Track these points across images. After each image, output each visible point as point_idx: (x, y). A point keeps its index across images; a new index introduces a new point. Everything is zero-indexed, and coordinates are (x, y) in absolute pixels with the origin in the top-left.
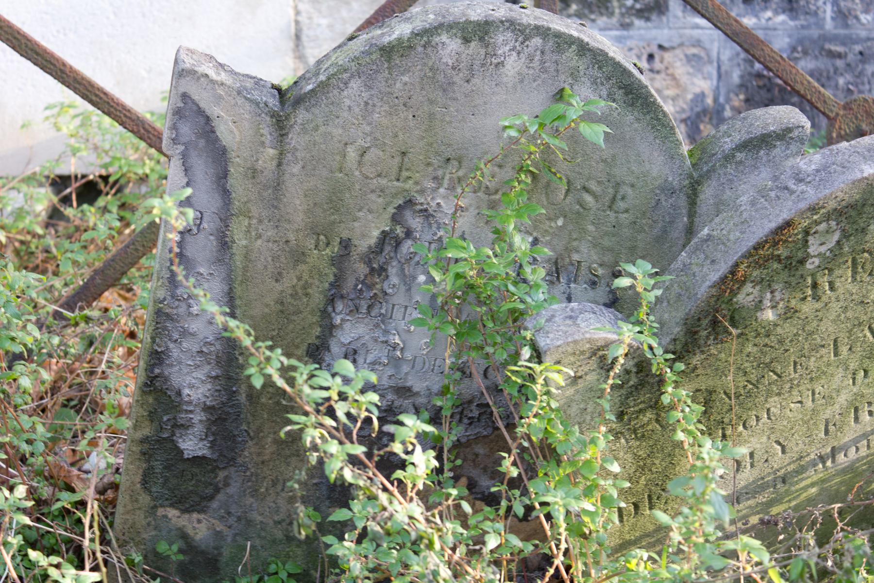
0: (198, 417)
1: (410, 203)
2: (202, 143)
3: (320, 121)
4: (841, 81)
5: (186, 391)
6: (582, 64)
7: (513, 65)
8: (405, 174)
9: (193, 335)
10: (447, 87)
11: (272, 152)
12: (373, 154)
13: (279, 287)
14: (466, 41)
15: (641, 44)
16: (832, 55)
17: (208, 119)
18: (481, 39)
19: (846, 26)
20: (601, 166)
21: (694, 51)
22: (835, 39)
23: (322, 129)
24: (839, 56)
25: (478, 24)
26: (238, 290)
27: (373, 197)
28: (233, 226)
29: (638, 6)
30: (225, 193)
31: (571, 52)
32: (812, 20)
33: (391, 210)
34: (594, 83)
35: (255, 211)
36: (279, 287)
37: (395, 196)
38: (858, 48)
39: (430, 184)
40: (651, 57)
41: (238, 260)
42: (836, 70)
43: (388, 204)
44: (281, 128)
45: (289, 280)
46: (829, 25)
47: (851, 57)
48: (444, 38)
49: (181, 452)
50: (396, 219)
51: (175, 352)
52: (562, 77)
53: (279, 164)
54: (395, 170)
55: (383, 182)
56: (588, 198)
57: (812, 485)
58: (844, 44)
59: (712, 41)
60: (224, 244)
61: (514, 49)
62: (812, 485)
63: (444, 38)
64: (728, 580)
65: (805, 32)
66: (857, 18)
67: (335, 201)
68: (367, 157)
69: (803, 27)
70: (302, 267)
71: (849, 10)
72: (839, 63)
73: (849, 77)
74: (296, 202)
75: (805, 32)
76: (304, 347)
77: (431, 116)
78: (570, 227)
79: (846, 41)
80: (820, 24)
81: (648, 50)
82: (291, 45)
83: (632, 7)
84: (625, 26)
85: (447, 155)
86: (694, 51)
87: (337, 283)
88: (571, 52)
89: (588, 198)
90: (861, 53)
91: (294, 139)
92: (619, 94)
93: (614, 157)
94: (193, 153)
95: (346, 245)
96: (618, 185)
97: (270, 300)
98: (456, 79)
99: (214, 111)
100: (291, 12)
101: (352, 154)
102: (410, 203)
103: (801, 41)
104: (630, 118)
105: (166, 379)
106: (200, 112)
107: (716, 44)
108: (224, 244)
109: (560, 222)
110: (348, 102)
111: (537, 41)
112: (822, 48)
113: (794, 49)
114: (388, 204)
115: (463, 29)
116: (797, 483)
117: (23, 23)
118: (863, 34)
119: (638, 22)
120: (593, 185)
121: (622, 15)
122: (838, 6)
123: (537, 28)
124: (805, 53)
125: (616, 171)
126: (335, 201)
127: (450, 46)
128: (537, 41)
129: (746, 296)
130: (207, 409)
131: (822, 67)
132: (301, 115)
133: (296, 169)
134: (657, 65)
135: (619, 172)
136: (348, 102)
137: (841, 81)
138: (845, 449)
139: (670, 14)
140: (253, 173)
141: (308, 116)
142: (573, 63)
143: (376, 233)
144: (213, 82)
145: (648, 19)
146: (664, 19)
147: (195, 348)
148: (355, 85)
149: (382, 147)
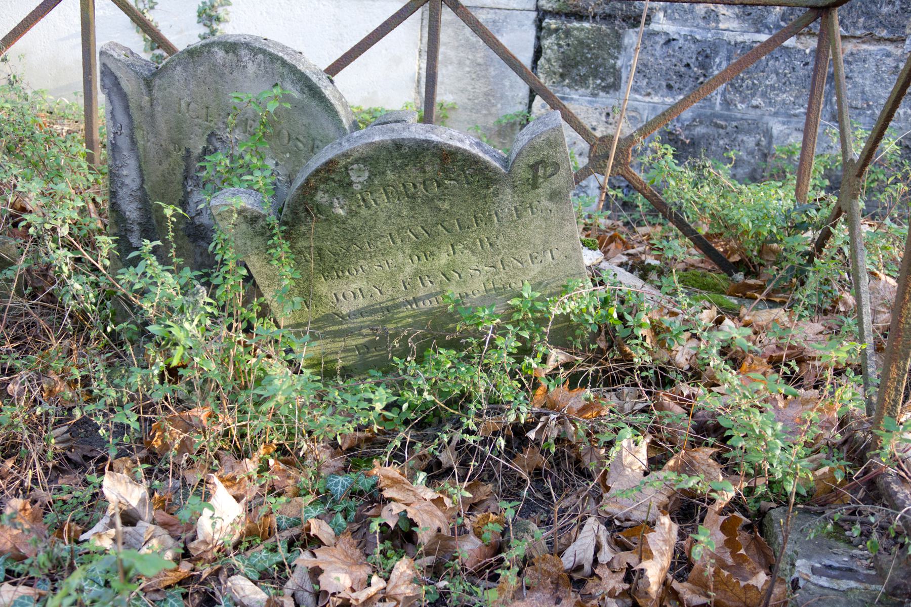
0: (136, 227)
1: (213, 134)
2: (115, 89)
3: (166, 85)
4: (721, 142)
5: (128, 213)
6: (285, 71)
7: (251, 68)
8: (210, 118)
9: (127, 185)
10: (222, 75)
11: (147, 98)
12: (193, 105)
13: (161, 168)
14: (227, 52)
15: (602, 106)
16: (718, 126)
17: (116, 77)
18: (234, 52)
19: (729, 110)
20: (303, 128)
21: (634, 114)
22: (720, 116)
23: (168, 90)
24: (722, 127)
25: (231, 43)
26: (144, 167)
27: (196, 128)
28: (136, 133)
29: (603, 84)
30: (130, 116)
31: (278, 64)
32: (707, 103)
33: (206, 136)
34: (293, 82)
35: (145, 127)
36: (161, 168)
37: (206, 129)
38: (734, 124)
39: (222, 126)
40: (608, 114)
41: (141, 150)
42: (719, 135)
43: (204, 133)
44: (149, 87)
45: (165, 166)
46: (718, 108)
47: (729, 129)
48: (216, 49)
49: (131, 244)
50: (209, 141)
51: (121, 193)
52: (276, 77)
53: (152, 105)
54: (204, 115)
55: (200, 121)
56: (300, 145)
57: (408, 317)
58: (726, 120)
59: (644, 110)
60: (134, 143)
61: (250, 59)
62: (408, 317)
63: (216, 49)
64: (907, 492)
65: (703, 111)
66: (735, 105)
67: (179, 129)
68: (191, 107)
69: (701, 107)
70: (170, 159)
71: (731, 100)
72: (721, 131)
73: (727, 141)
74: (162, 126)
75: (703, 111)
76: (177, 201)
77: (217, 90)
78: (293, 159)
79: (728, 119)
80: (712, 106)
81: (607, 111)
82: (415, 85)
83: (600, 85)
84: (594, 95)
85: (228, 111)
86: (634, 114)
87: (187, 170)
88: (278, 64)
89: (300, 145)
90: (736, 127)
91: (156, 93)
92: (306, 90)
93: (309, 124)
94: (112, 94)
95: (188, 151)
96: (313, 140)
97: (158, 174)
98: (225, 72)
99: (118, 74)
100: (417, 68)
101: (183, 105)
102: (213, 134)
103: (699, 116)
104: (314, 104)
105: (119, 206)
106: (112, 74)
107: (646, 112)
108: (134, 143)
109: (288, 155)
110: (177, 77)
111: (260, 56)
112: (712, 122)
113: (694, 120)
114: (204, 133)
115: (224, 46)
116: (397, 313)
117: (442, 83)
118: (739, 116)
119: (601, 94)
120: (301, 138)
121: (594, 88)
122: (725, 97)
123: (260, 49)
124: (701, 123)
125: (311, 132)
126: (179, 129)
127: (220, 54)
128: (260, 56)
129: (321, 197)
130: (139, 224)
131: (711, 132)
132: (157, 82)
133: (159, 109)
134: (611, 120)
135: (314, 133)
136: (177, 77)
137: (721, 142)
138: (422, 299)
139: (621, 91)
140: (141, 108)
141: (161, 82)
142: (280, 70)
143: (201, 147)
144: (116, 59)
145: (608, 93)
146: (617, 93)
147: (129, 192)
148: (179, 68)
149: (196, 102)
